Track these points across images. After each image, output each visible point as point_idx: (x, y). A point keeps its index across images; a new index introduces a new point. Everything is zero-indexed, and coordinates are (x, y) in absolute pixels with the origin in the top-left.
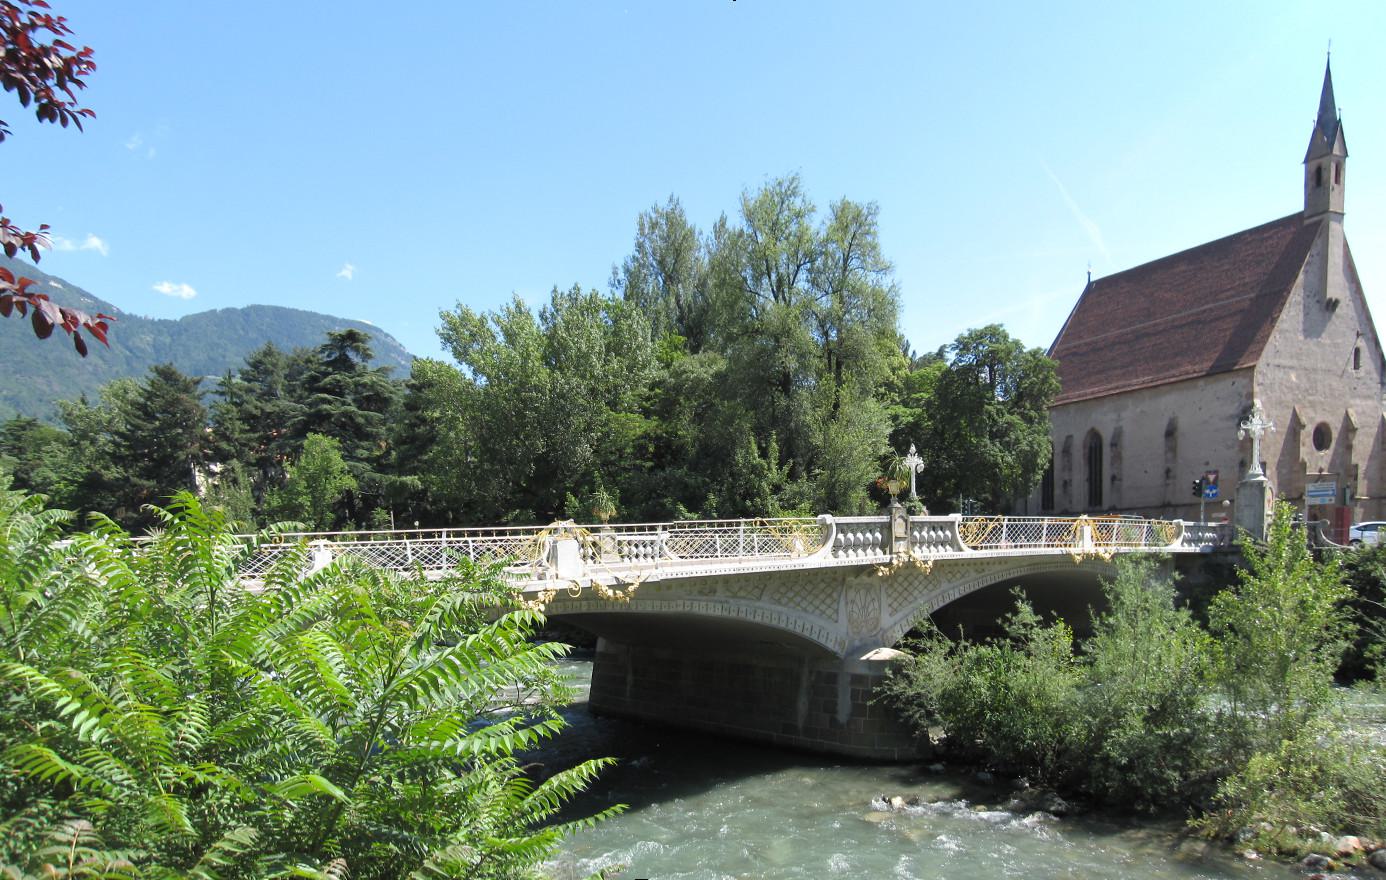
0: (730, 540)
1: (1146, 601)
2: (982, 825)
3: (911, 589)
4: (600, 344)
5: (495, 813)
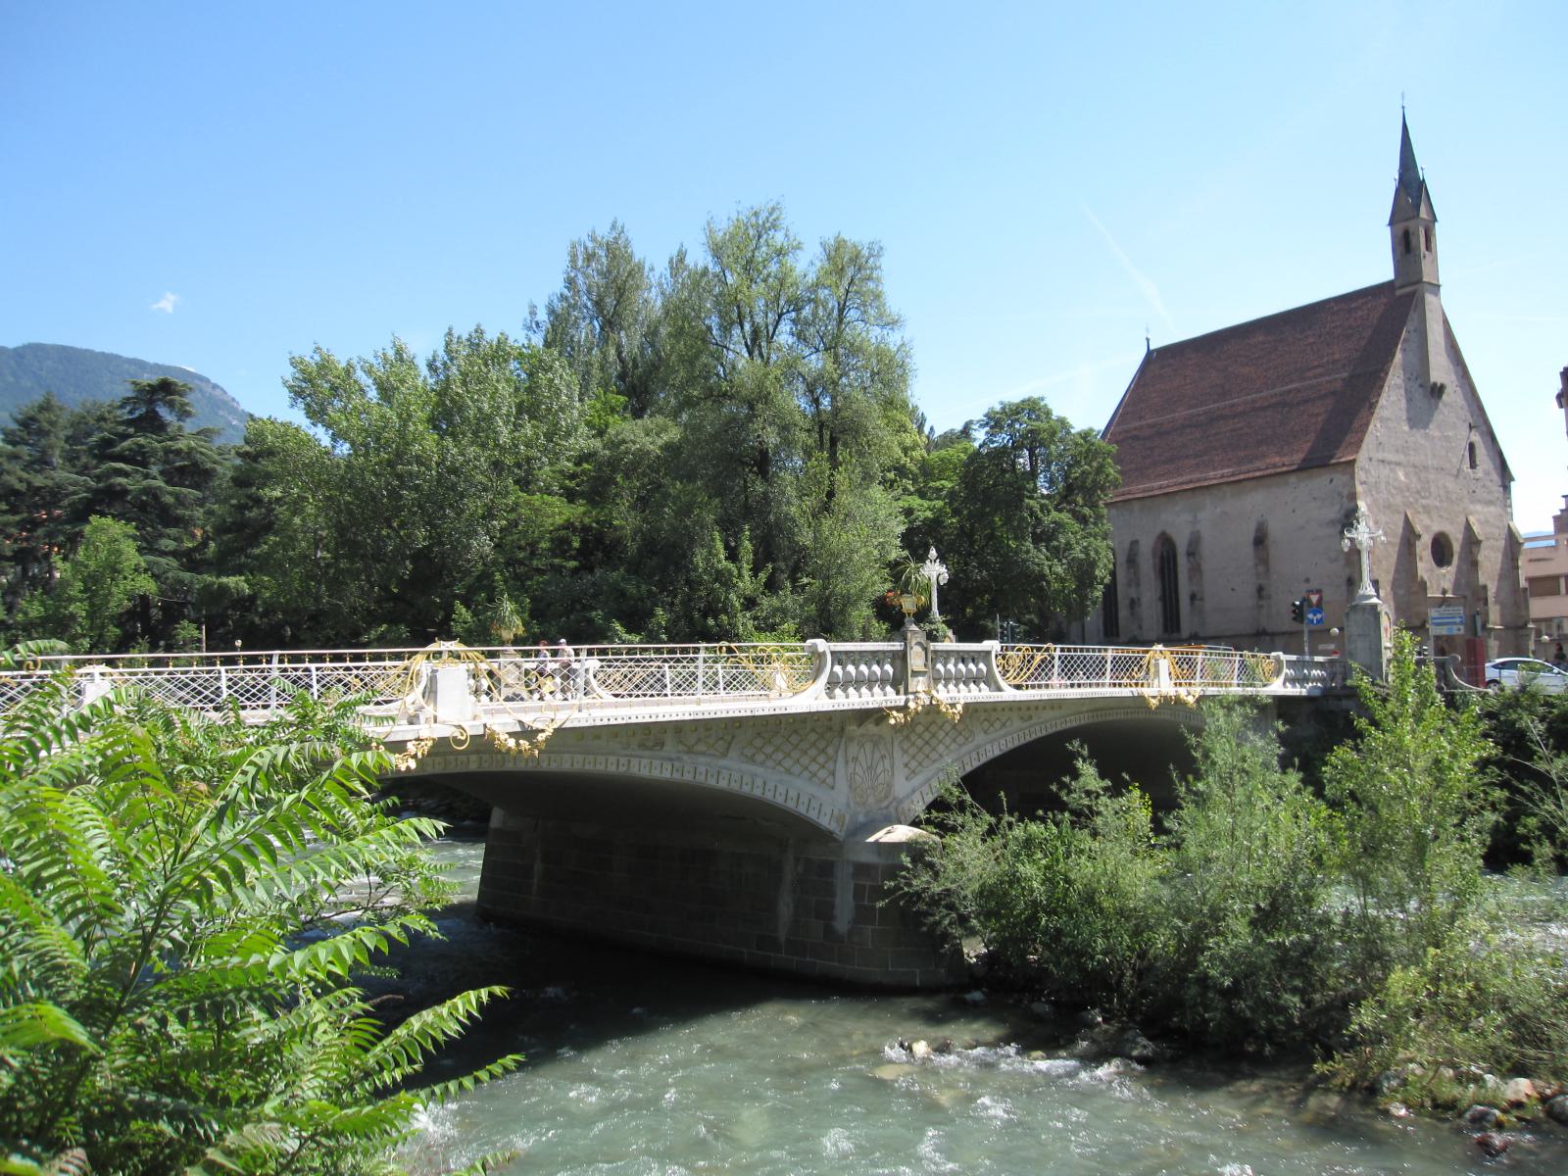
0: (684, 672)
1: (1244, 759)
2: (1040, 1079)
3: (934, 742)
4: (508, 405)
5: (324, 1073)
